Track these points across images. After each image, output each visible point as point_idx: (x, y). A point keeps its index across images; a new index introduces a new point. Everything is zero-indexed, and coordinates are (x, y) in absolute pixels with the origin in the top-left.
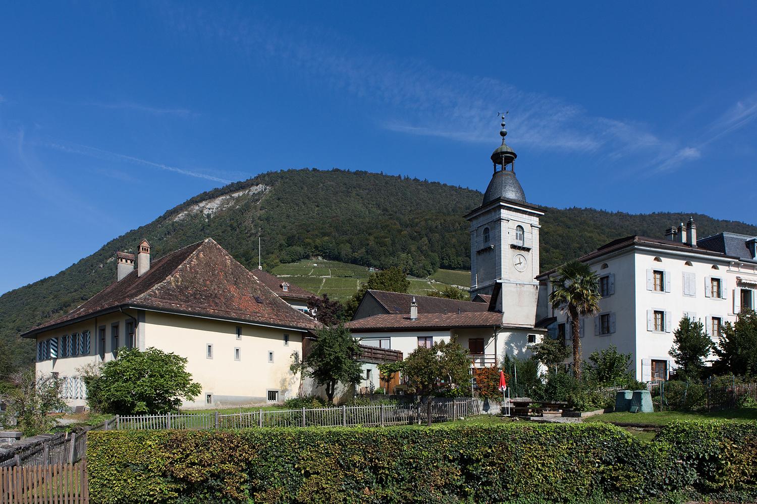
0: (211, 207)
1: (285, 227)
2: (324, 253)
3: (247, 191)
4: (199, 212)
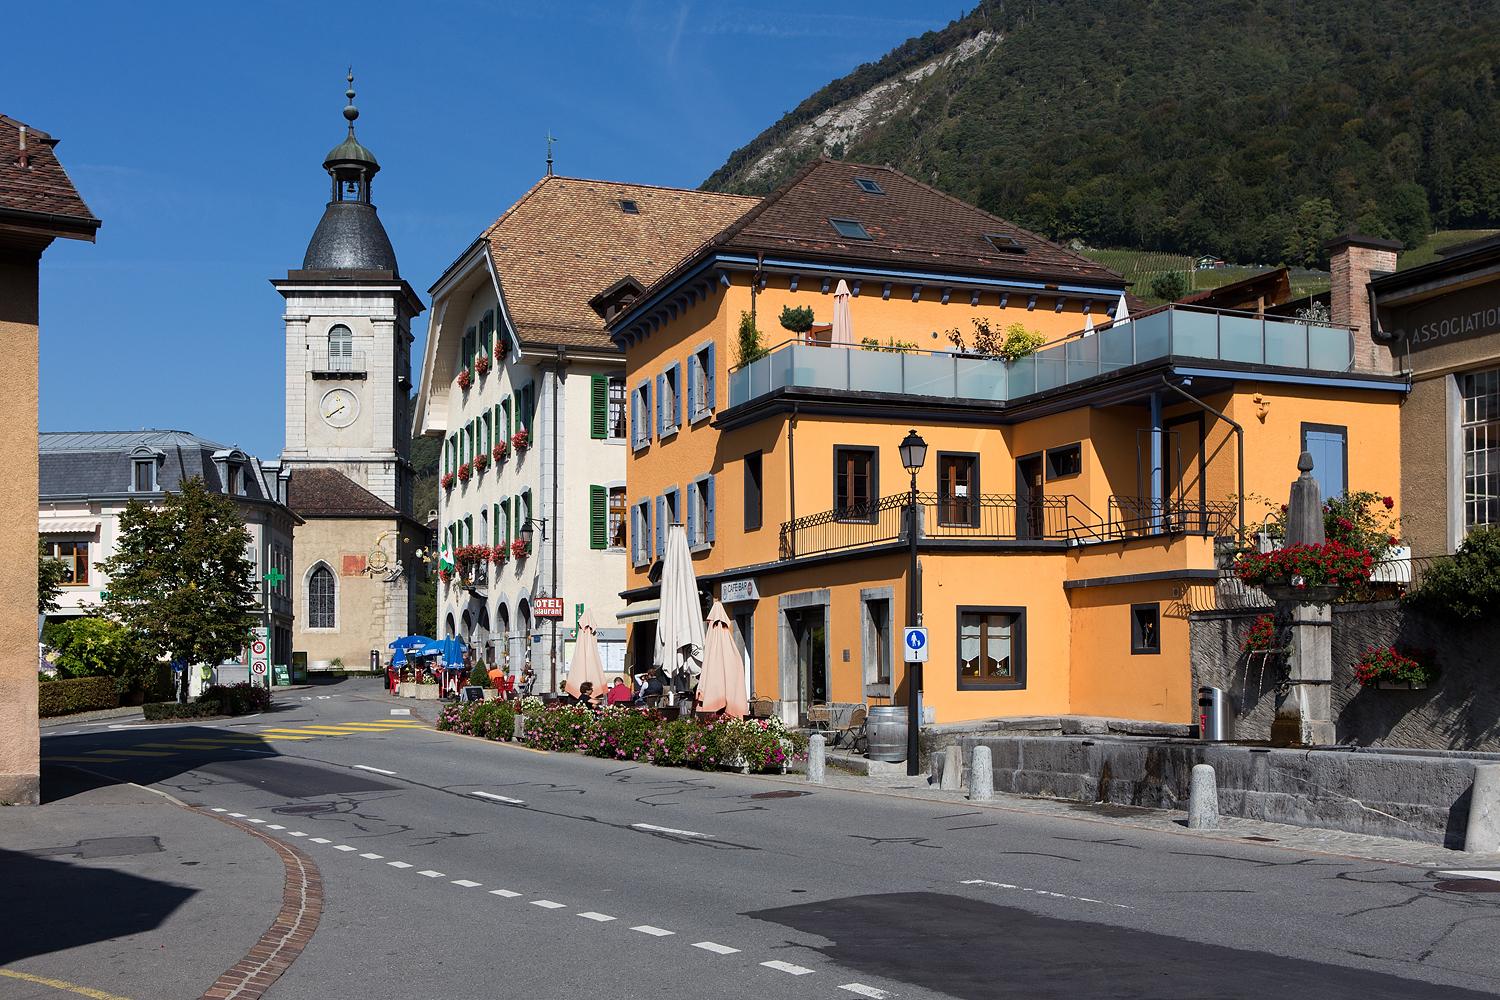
0: (847, 122)
1: (998, 161)
2: (1091, 226)
3: (948, 58)
4: (813, 144)
